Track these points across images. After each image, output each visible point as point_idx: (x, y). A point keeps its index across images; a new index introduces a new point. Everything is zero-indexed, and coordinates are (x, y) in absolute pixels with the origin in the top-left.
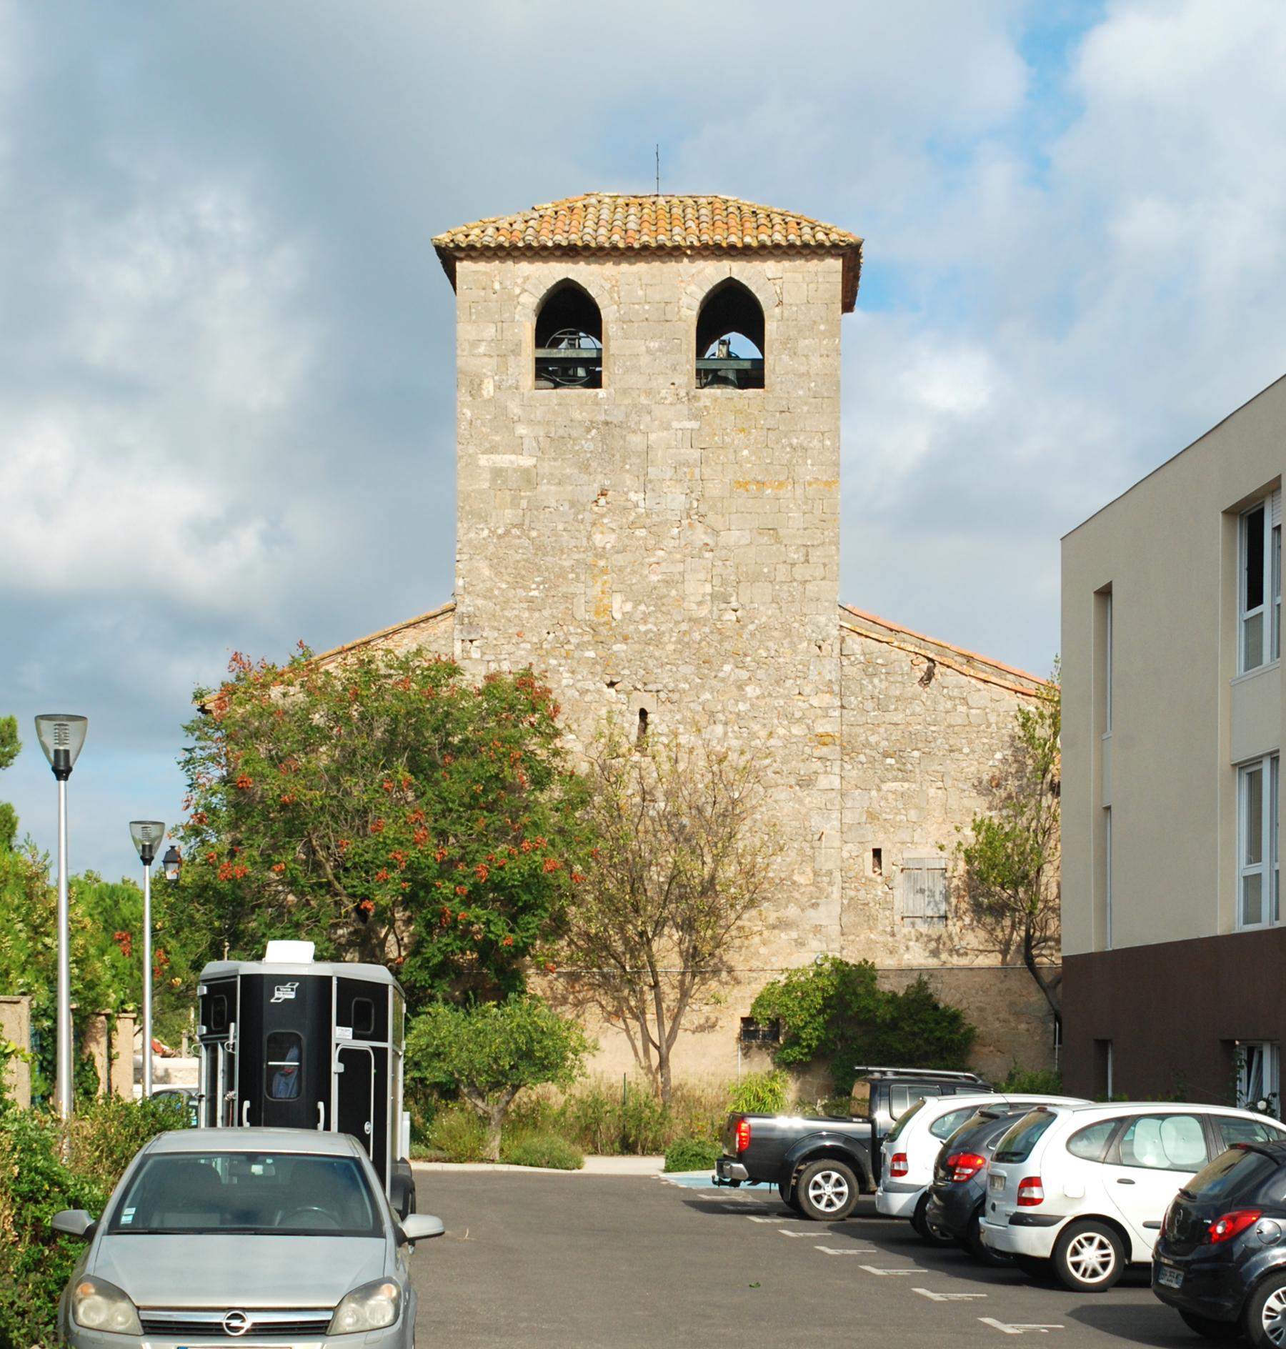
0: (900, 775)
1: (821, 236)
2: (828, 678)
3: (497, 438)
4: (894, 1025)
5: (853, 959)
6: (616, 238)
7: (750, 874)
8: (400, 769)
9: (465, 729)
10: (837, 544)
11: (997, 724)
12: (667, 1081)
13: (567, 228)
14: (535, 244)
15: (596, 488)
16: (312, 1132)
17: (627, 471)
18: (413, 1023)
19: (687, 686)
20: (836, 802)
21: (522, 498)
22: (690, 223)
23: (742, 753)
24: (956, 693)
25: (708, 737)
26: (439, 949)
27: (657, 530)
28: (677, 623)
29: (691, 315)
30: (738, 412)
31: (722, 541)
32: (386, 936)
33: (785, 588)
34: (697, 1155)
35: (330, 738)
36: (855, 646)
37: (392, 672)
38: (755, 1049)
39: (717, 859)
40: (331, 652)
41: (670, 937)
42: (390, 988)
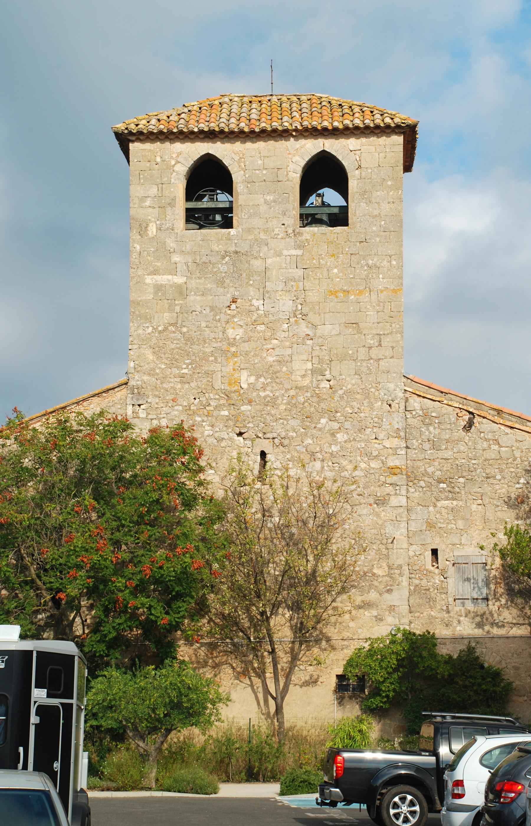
0: (450, 495)
1: (388, 120)
2: (396, 427)
3: (159, 264)
4: (450, 680)
5: (418, 629)
6: (242, 125)
7: (342, 568)
8: (87, 497)
9: (135, 468)
10: (401, 333)
11: (521, 458)
12: (281, 724)
13: (208, 119)
14: (185, 130)
15: (229, 297)
16: (14, 771)
18: (93, 684)
19: (295, 434)
20: (404, 516)
21: (176, 305)
22: (295, 114)
23: (335, 481)
24: (490, 436)
25: (310, 470)
26: (113, 627)
27: (272, 327)
28: (287, 390)
29: (296, 177)
32: (74, 618)
33: (364, 364)
34: (304, 781)
35: (36, 476)
36: (416, 404)
37: (82, 428)
38: (347, 698)
39: (317, 558)
40: (38, 415)
41: (283, 615)
42: (76, 658)
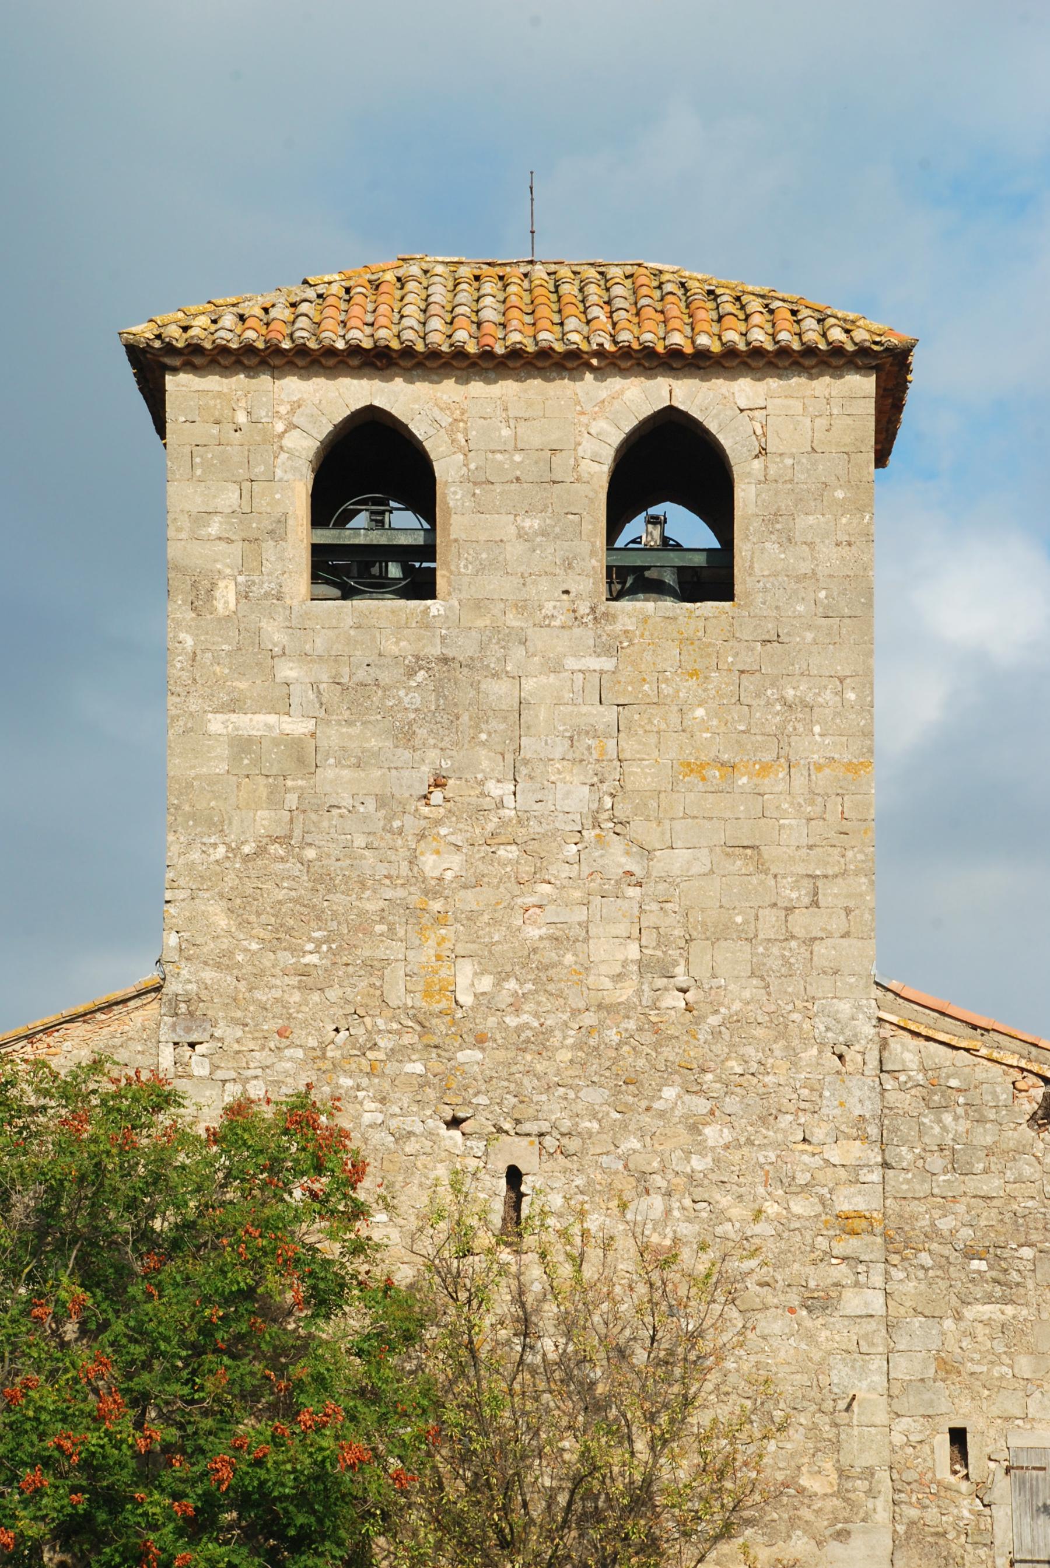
1: (836, 334)
2: (857, 1113)
3: (243, 685)
6: (461, 335)
13: (369, 318)
14: (312, 345)
15: (426, 774)
17: (483, 744)
19: (595, 1126)
22: (595, 311)
27: (537, 854)
28: (575, 1012)
29: (598, 472)
30: (685, 641)
31: (658, 867)
33: (775, 950)
36: (908, 1056)
39: (659, 1444)
